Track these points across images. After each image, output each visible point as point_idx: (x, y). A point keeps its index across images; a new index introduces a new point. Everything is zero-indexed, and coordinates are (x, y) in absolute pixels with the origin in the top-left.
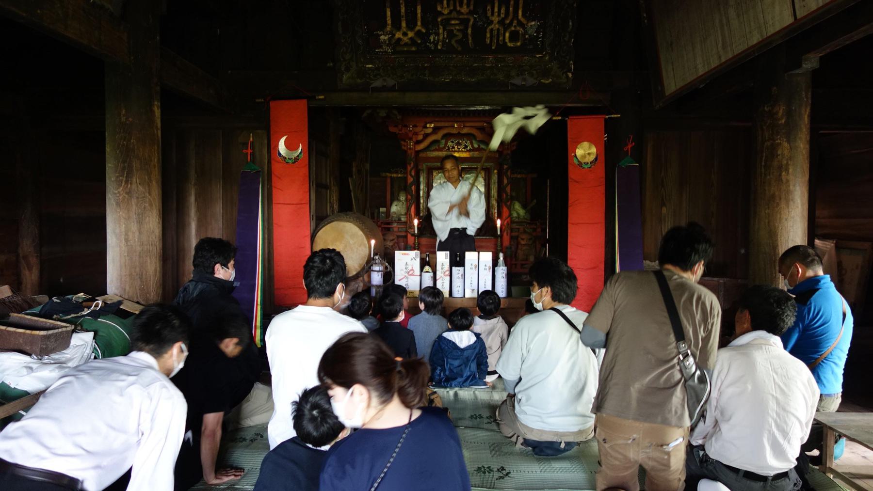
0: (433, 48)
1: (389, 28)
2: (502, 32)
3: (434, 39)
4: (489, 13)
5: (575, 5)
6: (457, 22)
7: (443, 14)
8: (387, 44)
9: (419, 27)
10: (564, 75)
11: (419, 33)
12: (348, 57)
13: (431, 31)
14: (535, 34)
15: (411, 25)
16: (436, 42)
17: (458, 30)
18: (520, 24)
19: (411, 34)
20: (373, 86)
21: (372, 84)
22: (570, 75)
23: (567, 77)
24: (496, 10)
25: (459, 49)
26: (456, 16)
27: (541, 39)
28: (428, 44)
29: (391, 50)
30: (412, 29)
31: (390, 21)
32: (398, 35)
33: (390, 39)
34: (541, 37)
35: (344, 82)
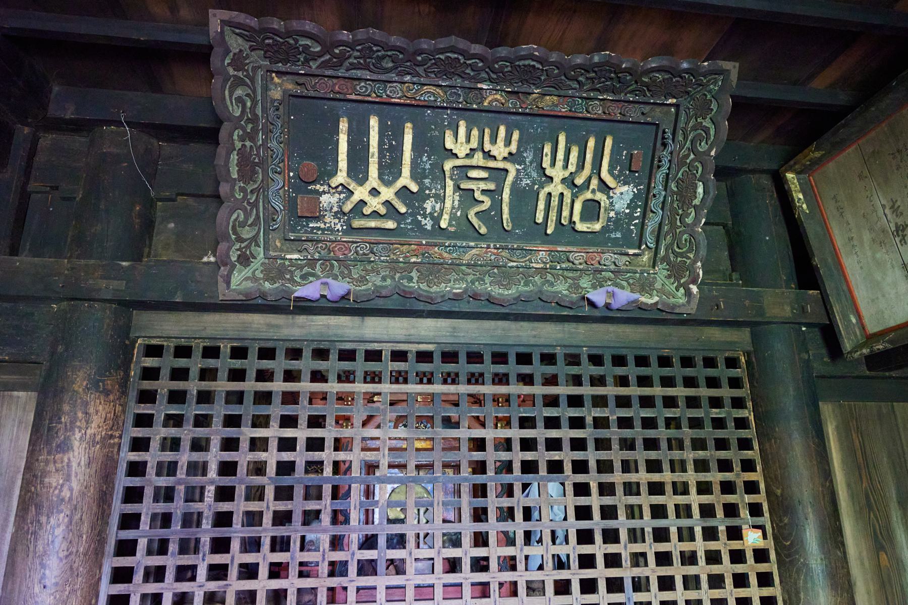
0: (429, 227)
1: (341, 177)
2: (569, 201)
3: (433, 208)
4: (546, 163)
5: (713, 153)
6: (484, 174)
7: (456, 156)
8: (335, 213)
9: (405, 179)
10: (682, 290)
11: (404, 193)
12: (247, 233)
13: (427, 192)
14: (627, 211)
15: (390, 171)
16: (436, 214)
17: (484, 192)
18: (604, 187)
19: (388, 193)
20: (296, 294)
21: (296, 291)
22: (694, 289)
23: (688, 293)
24: (560, 155)
25: (483, 230)
26: (482, 163)
27: (637, 221)
28: (419, 218)
29: (342, 226)
30: (388, 184)
31: (346, 162)
32: (361, 192)
33: (341, 203)
34: (637, 218)
35: (233, 286)
